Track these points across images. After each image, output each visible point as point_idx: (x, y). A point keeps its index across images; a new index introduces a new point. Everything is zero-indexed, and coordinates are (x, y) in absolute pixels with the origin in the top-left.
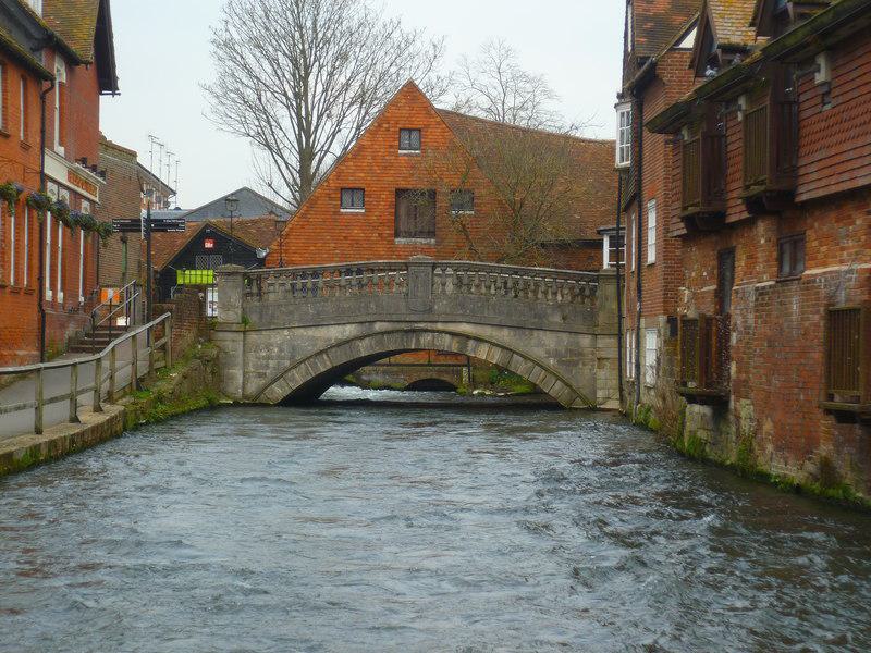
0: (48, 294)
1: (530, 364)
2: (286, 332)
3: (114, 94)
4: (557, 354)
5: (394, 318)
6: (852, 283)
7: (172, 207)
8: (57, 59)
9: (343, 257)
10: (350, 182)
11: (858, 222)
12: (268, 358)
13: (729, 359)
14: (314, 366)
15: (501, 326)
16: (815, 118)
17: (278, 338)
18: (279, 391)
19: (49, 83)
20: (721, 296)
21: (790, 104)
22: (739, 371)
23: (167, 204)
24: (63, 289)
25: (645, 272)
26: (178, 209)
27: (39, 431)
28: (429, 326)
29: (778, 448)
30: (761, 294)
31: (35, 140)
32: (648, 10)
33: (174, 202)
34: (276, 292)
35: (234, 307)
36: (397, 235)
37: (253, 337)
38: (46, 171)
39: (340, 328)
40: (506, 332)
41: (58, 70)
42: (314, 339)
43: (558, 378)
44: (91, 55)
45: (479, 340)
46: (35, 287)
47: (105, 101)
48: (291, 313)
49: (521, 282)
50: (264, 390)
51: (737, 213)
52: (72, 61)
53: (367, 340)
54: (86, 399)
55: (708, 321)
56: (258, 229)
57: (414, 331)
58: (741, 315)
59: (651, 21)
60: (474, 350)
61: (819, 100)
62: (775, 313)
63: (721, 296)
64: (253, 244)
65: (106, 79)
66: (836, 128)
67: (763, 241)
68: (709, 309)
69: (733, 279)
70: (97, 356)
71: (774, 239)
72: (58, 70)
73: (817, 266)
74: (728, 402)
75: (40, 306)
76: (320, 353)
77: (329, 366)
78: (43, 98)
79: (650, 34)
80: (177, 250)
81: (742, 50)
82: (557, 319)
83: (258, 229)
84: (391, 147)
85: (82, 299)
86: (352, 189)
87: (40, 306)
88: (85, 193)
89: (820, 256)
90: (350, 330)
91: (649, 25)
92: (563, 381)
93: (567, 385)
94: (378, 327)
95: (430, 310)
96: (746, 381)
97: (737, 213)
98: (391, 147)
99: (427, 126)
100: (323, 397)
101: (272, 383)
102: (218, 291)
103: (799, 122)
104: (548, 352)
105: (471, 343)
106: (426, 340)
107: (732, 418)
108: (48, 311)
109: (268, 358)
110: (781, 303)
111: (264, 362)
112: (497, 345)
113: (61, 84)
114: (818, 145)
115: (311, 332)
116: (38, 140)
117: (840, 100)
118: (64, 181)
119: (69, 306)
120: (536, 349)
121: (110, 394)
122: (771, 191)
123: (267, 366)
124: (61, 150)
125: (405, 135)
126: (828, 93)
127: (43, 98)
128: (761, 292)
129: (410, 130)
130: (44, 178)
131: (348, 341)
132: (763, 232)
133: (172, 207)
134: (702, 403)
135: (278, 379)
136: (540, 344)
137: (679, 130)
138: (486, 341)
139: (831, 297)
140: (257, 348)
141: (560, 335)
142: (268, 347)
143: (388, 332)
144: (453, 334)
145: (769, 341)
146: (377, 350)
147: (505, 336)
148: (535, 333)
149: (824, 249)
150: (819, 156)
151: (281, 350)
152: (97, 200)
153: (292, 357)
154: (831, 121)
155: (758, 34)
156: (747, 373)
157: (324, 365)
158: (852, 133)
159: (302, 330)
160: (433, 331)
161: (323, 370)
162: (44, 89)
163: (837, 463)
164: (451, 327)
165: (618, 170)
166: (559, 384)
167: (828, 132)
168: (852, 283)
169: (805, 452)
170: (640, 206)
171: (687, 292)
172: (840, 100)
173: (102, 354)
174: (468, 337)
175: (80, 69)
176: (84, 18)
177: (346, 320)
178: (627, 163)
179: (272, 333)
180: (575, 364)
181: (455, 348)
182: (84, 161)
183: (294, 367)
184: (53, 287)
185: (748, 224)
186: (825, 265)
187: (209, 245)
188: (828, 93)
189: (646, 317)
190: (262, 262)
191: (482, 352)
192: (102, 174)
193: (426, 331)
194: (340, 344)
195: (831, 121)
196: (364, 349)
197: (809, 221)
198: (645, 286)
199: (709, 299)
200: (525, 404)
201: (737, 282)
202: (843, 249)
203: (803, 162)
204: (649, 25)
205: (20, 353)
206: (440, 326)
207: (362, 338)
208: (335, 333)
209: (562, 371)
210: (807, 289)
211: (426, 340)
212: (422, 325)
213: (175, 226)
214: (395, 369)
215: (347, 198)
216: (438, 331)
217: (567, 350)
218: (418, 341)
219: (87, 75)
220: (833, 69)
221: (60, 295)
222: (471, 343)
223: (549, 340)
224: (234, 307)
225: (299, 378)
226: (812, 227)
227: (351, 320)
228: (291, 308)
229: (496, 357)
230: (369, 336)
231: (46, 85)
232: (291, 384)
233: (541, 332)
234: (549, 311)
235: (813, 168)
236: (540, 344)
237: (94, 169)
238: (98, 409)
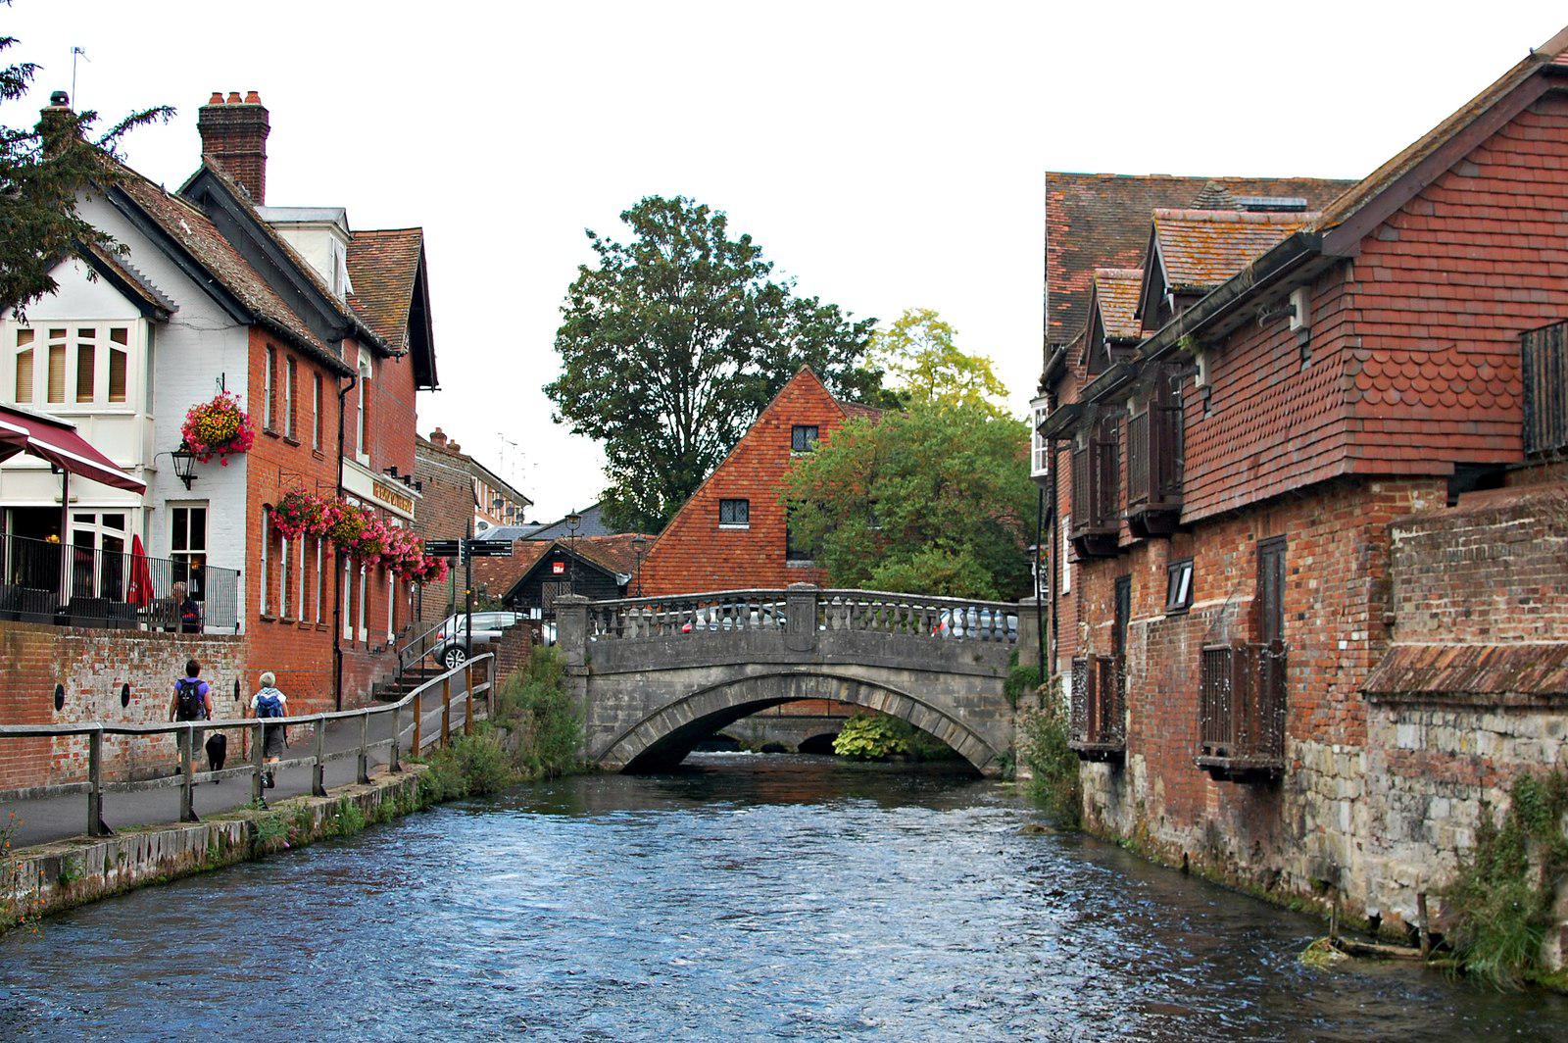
0: (347, 632)
1: (935, 715)
2: (638, 677)
3: (433, 390)
4: (968, 703)
5: (770, 659)
6: (1234, 618)
7: (528, 520)
8: (360, 350)
9: (724, 584)
10: (732, 492)
11: (1241, 548)
12: (617, 708)
13: (1122, 709)
14: (672, 718)
15: (899, 669)
16: (1198, 428)
17: (628, 683)
18: (631, 749)
19: (349, 380)
20: (1118, 634)
21: (1175, 409)
22: (1133, 722)
23: (521, 516)
24: (366, 625)
25: (1060, 601)
26: (535, 523)
27: (319, 792)
28: (813, 669)
29: (1169, 811)
30: (1152, 631)
31: (331, 447)
32: (1065, 289)
33: (530, 514)
34: (635, 623)
35: (576, 646)
36: (790, 555)
37: (599, 682)
38: (344, 484)
39: (704, 672)
40: (905, 677)
41: (362, 364)
42: (670, 685)
43: (969, 733)
44: (404, 346)
45: (872, 686)
46: (330, 622)
47: (423, 397)
48: (645, 653)
49: (910, 613)
50: (609, 750)
51: (1127, 539)
52: (378, 353)
53: (736, 687)
54: (382, 755)
55: (1105, 663)
56: (621, 550)
57: (793, 675)
58: (1136, 655)
59: (1067, 301)
60: (867, 698)
61: (1200, 406)
62: (1165, 654)
63: (1118, 634)
64: (612, 569)
65: (424, 373)
66: (1216, 439)
67: (1154, 569)
68: (1105, 649)
69: (1128, 613)
70: (395, 705)
71: (1164, 566)
72: (362, 364)
73: (1204, 598)
74: (1123, 758)
75: (336, 644)
76: (680, 702)
77: (691, 717)
78: (341, 397)
79: (1065, 316)
80: (521, 575)
81: (1129, 344)
82: (967, 659)
83: (621, 550)
84: (781, 448)
85: (391, 637)
86: (734, 501)
87: (336, 644)
88: (396, 509)
89: (1206, 586)
90: (716, 675)
91: (1065, 306)
92: (974, 736)
93: (981, 741)
94: (749, 670)
95: (814, 649)
96: (1139, 734)
97: (1127, 539)
98: (781, 448)
99: (826, 423)
100: (687, 761)
101: (623, 738)
102: (557, 629)
103: (1184, 430)
104: (957, 701)
105: (863, 690)
106: (808, 686)
107: (1128, 778)
108: (346, 651)
109: (617, 708)
110: (1171, 642)
111: (612, 713)
112: (895, 693)
113: (365, 380)
114: (1200, 459)
115: (667, 677)
116: (335, 448)
117: (1221, 406)
118: (369, 495)
119: (375, 644)
120: (942, 698)
121: (413, 750)
122: (1152, 511)
123: (616, 718)
124: (365, 459)
125: (799, 434)
126: (1208, 398)
127: (341, 397)
128: (1153, 629)
129: (805, 428)
130: (341, 491)
131: (714, 688)
132: (1155, 553)
133: (528, 520)
134: (1095, 759)
135: (629, 733)
136: (947, 692)
137: (1074, 435)
138: (881, 687)
139: (1214, 634)
140: (603, 697)
141: (972, 679)
142: (616, 694)
143: (763, 677)
144: (841, 679)
145: (1160, 686)
146: (749, 699)
147: (904, 680)
148: (942, 677)
149: (1210, 578)
150: (1201, 471)
151: (632, 698)
152: (411, 516)
153: (645, 708)
154: (1212, 431)
155: (1143, 328)
156: (1141, 723)
157: (683, 718)
158: (1232, 445)
159: (657, 675)
160: (817, 675)
161: (683, 723)
162: (343, 387)
163: (1221, 827)
164: (840, 671)
165: (1035, 479)
166: (971, 740)
167: (1209, 444)
168: (1234, 618)
169: (1194, 817)
170: (1055, 524)
171: (1087, 628)
172: (1221, 406)
173: (401, 703)
174: (860, 683)
175: (388, 363)
176: (396, 301)
177: (711, 661)
178: (1044, 472)
179: (621, 678)
180: (991, 715)
181: (843, 695)
182: (393, 472)
183: (649, 719)
184: (353, 623)
185: (1142, 547)
186: (1211, 596)
187: (558, 569)
188: (1208, 398)
189: (1062, 657)
190: (623, 591)
191: (877, 701)
192: (418, 486)
193: (809, 675)
194: (704, 691)
195: (1212, 431)
196: (733, 697)
197: (1197, 546)
198: (1061, 620)
199: (1106, 636)
200: (926, 772)
201: (1132, 617)
202: (1227, 579)
203: (1187, 477)
204: (1065, 306)
205: (311, 701)
206: (825, 670)
207: (731, 684)
208: (698, 678)
209: (974, 724)
210: (1194, 624)
211: (808, 686)
212: (803, 669)
213: (500, 548)
214: (785, 721)
215: (727, 513)
216: (823, 675)
217: (981, 698)
218: (799, 687)
219: (400, 368)
220: (1210, 372)
221: (363, 634)
222: (863, 690)
223: (958, 685)
224: (576, 646)
225: (654, 733)
226: (1200, 553)
227: (717, 661)
228: (645, 648)
229: (894, 707)
230: (739, 681)
231: (345, 382)
232: (644, 741)
233: (949, 678)
234: (958, 650)
235: (1196, 485)
236: (947, 692)
237: (407, 480)
238: (395, 769)
